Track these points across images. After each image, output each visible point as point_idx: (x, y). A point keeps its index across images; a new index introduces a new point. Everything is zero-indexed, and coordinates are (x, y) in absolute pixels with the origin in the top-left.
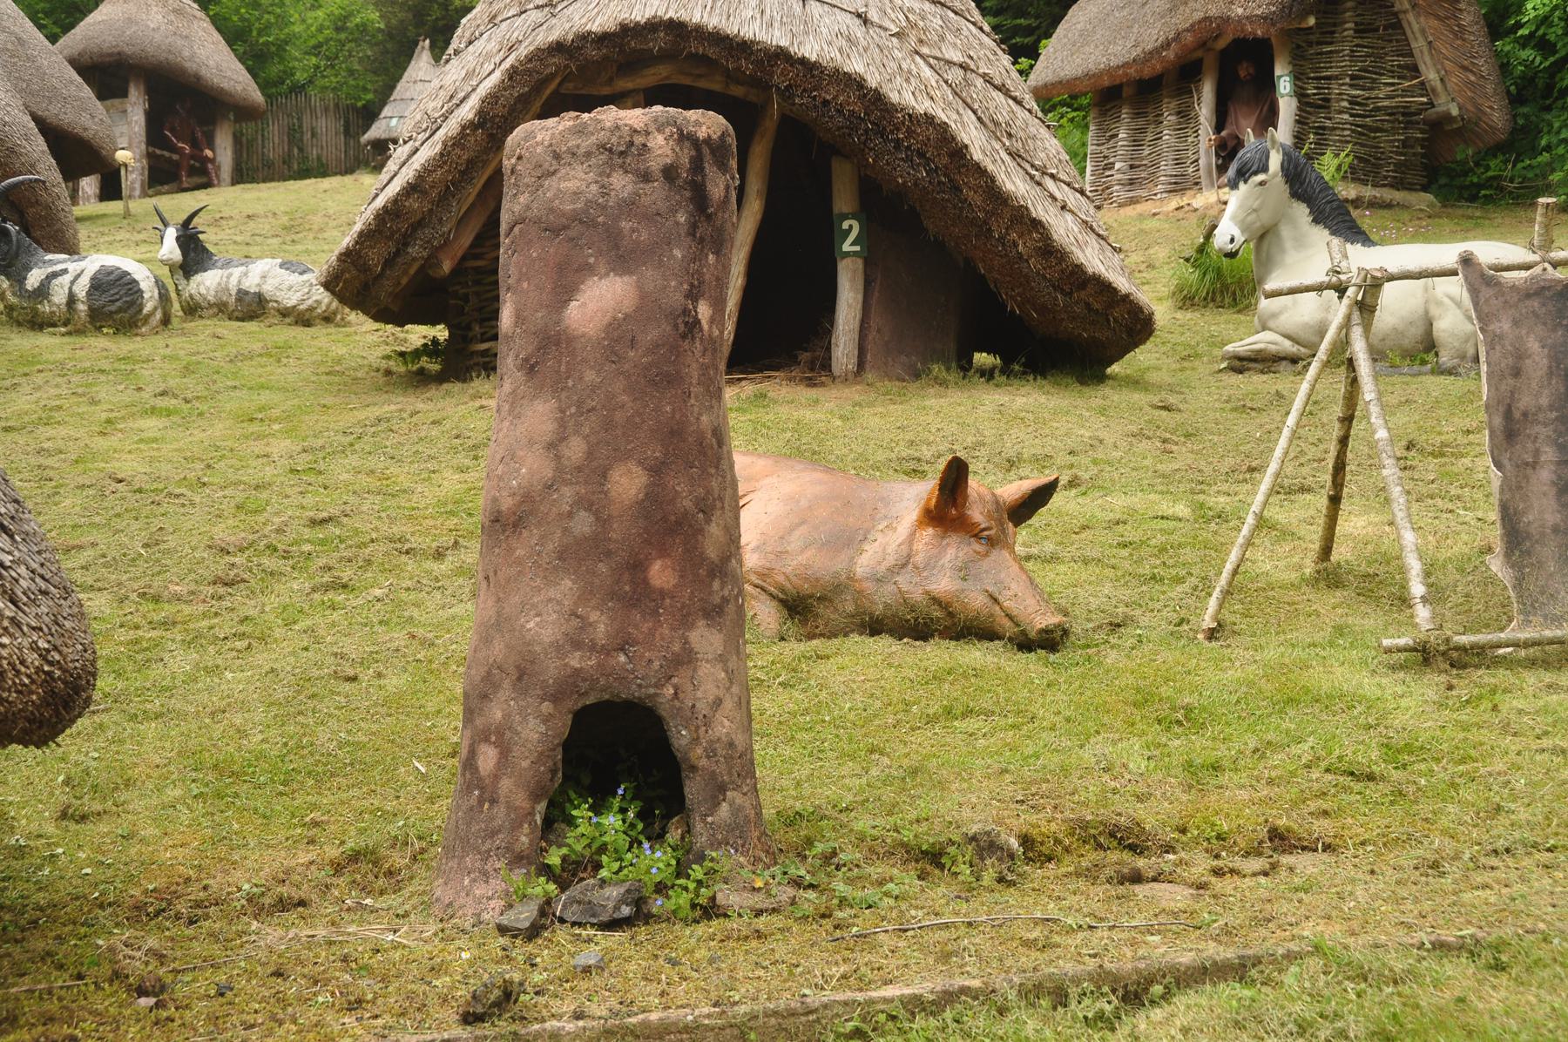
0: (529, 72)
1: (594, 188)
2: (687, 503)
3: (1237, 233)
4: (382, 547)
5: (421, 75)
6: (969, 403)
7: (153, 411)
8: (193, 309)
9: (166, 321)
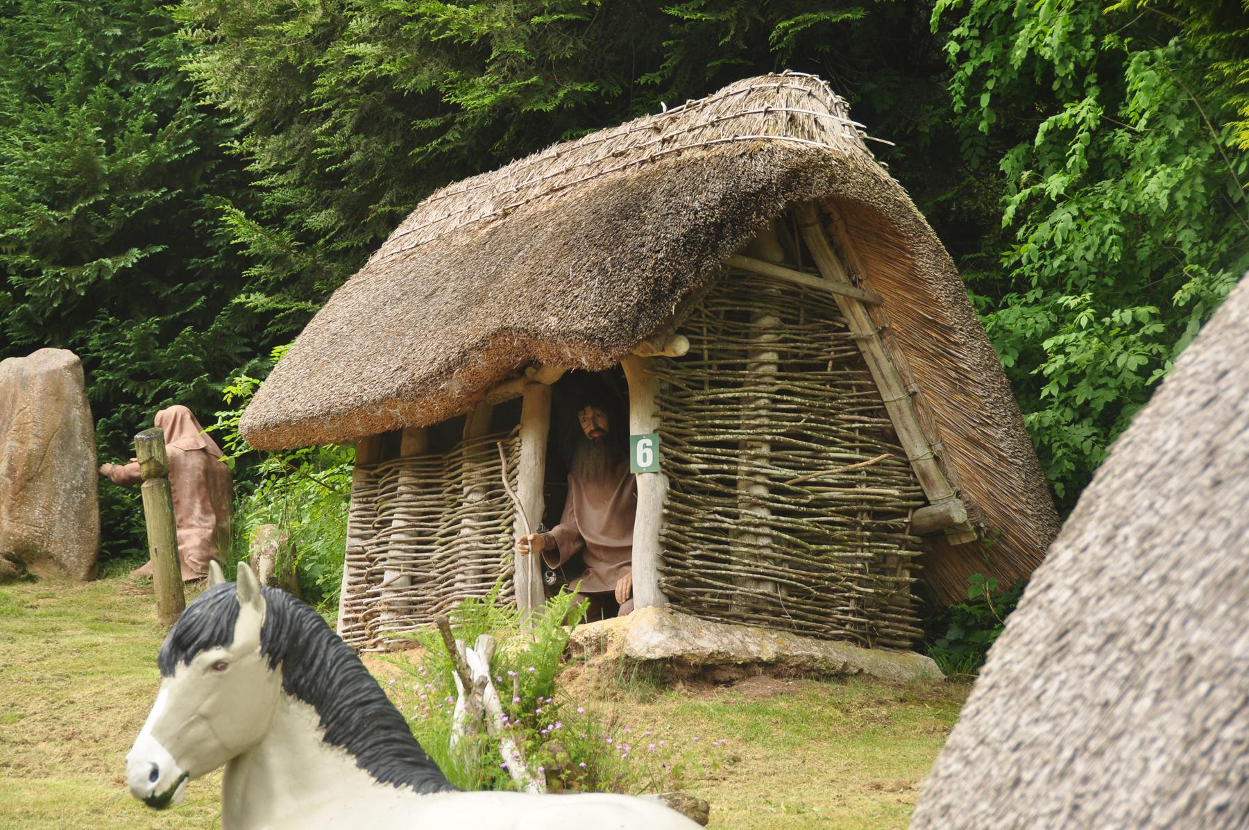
3: (164, 759)
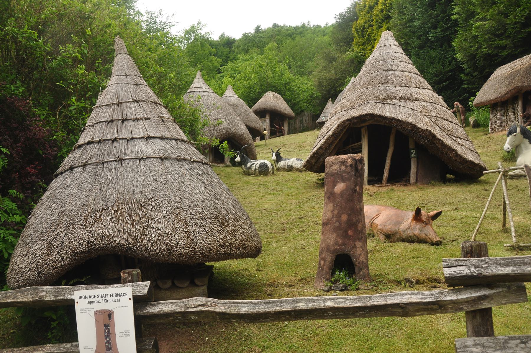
0: (342, 125)
2: (355, 221)
3: (509, 147)
4: (312, 223)
5: (329, 107)
6: (438, 190)
7: (271, 194)
8: (278, 169)
9: (273, 173)
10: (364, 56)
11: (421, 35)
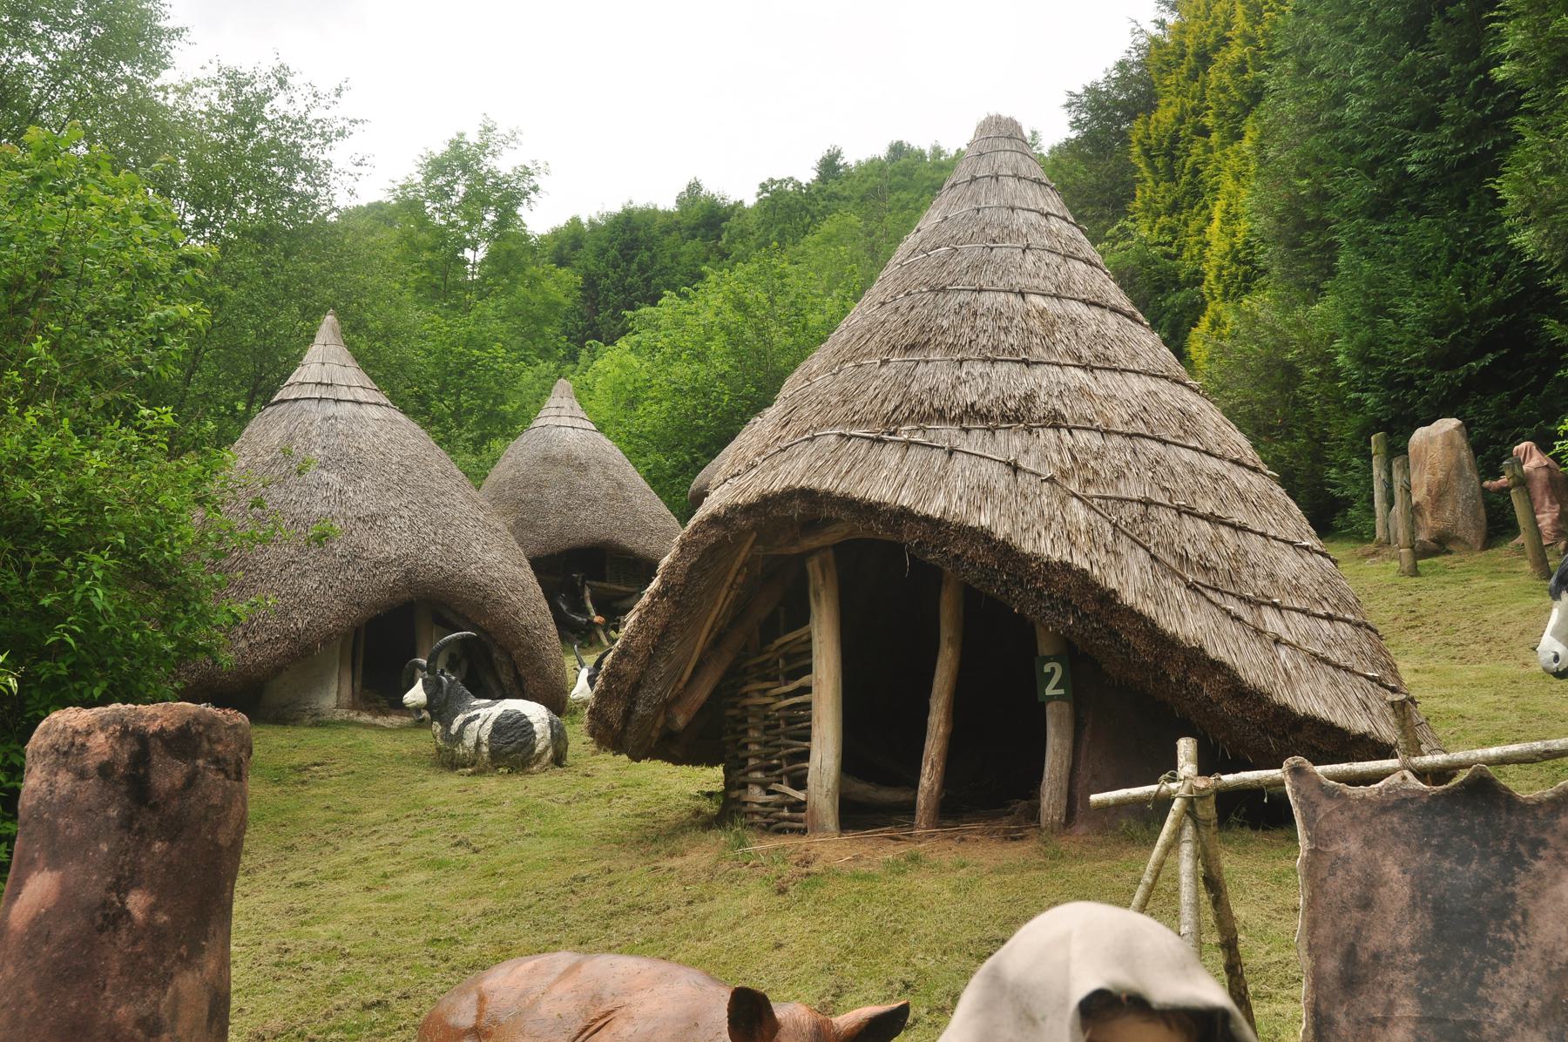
1: (45, 785)
9: (558, 760)
10: (1173, 257)
11: (1378, 161)
